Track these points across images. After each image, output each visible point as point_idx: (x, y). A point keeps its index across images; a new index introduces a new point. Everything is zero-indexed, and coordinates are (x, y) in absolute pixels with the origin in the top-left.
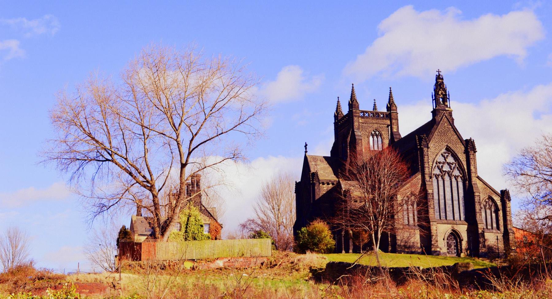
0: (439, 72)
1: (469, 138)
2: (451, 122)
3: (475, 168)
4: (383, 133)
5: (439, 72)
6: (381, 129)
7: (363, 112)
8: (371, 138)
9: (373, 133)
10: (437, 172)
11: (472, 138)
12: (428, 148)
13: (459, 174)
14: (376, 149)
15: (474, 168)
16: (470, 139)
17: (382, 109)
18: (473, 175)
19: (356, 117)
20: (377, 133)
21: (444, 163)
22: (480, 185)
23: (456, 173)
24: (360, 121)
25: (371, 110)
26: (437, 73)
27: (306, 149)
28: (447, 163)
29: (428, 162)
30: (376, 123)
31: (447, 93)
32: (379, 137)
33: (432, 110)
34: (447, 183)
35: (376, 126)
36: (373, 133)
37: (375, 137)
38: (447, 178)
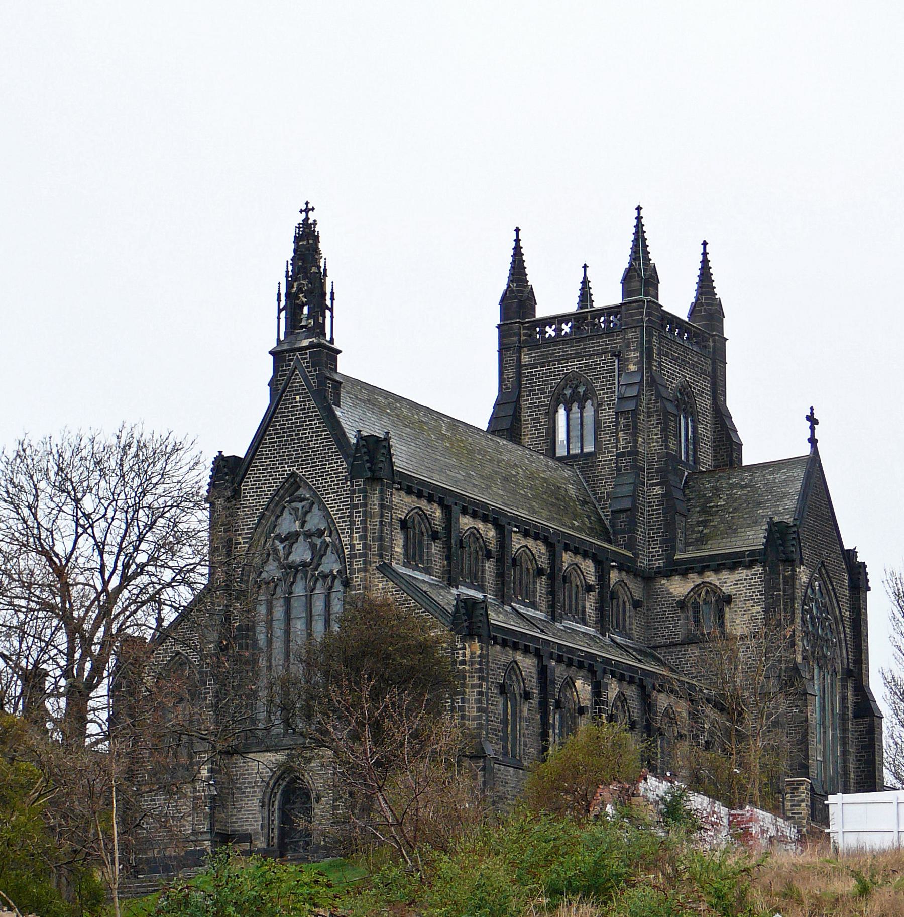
6: (590, 377)
24: (525, 359)
30: (578, 356)
33: (273, 344)
35: (573, 366)
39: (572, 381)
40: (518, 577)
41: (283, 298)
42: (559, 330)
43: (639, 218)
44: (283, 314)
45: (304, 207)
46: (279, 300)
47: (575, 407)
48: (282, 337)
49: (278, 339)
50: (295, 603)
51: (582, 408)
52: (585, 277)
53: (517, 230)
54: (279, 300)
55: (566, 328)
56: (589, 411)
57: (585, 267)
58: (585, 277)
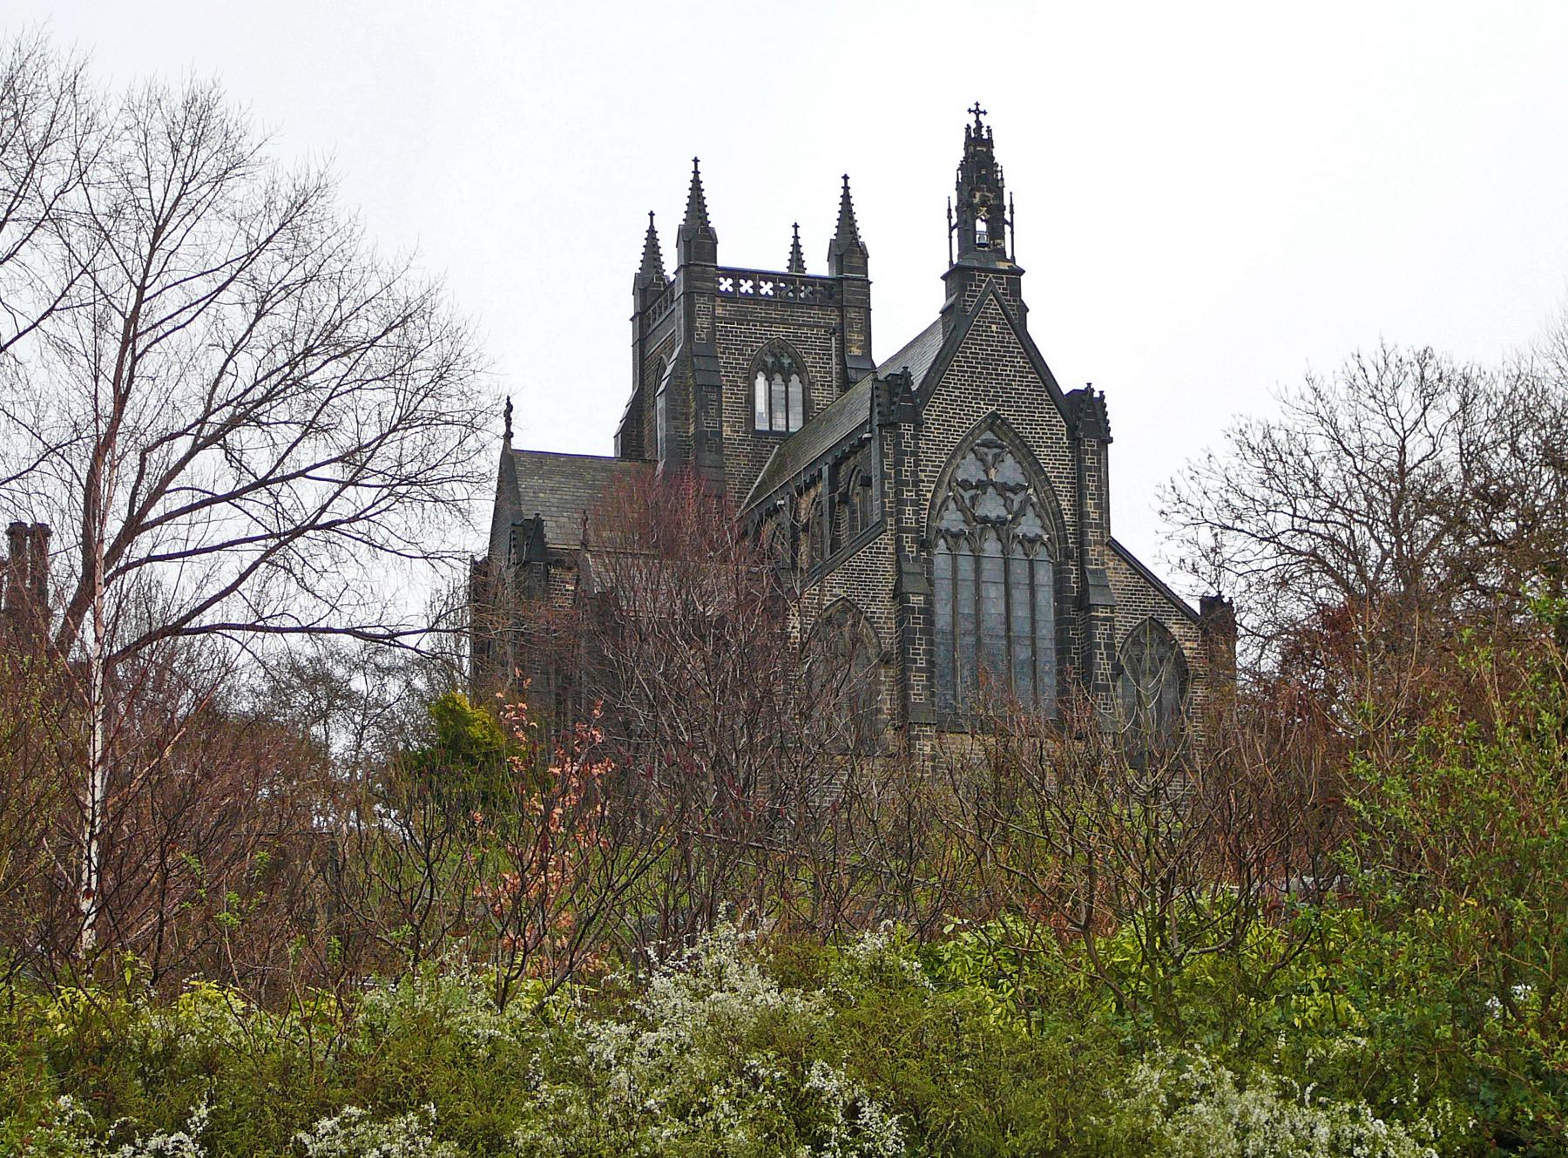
0: (977, 112)
1: (1082, 387)
2: (1017, 315)
3: (1104, 507)
4: (809, 360)
5: (977, 112)
6: (799, 348)
7: (737, 274)
8: (761, 383)
9: (770, 360)
10: (952, 519)
11: (1097, 388)
12: (919, 424)
13: (1039, 531)
14: (779, 424)
15: (1098, 506)
16: (1089, 389)
17: (817, 264)
18: (1092, 535)
19: (702, 294)
20: (786, 361)
21: (982, 486)
22: (1117, 576)
23: (1029, 526)
24: (719, 311)
25: (781, 265)
26: (971, 119)
27: (508, 424)
28: (994, 485)
29: (916, 483)
30: (783, 322)
31: (1007, 202)
32: (795, 378)
33: (946, 269)
34: (992, 570)
35: (779, 332)
36: (770, 360)
37: (778, 378)
38: (991, 547)
39: (778, 349)
40: (1020, 595)
41: (954, 214)
42: (756, 287)
43: (846, 188)
44: (955, 232)
45: (981, 108)
46: (950, 217)
47: (778, 378)
48: (955, 261)
49: (951, 262)
50: (986, 565)
51: (786, 382)
52: (652, 226)
53: (846, 178)
54: (950, 217)
55: (767, 288)
56: (795, 388)
57: (652, 214)
58: (652, 226)
